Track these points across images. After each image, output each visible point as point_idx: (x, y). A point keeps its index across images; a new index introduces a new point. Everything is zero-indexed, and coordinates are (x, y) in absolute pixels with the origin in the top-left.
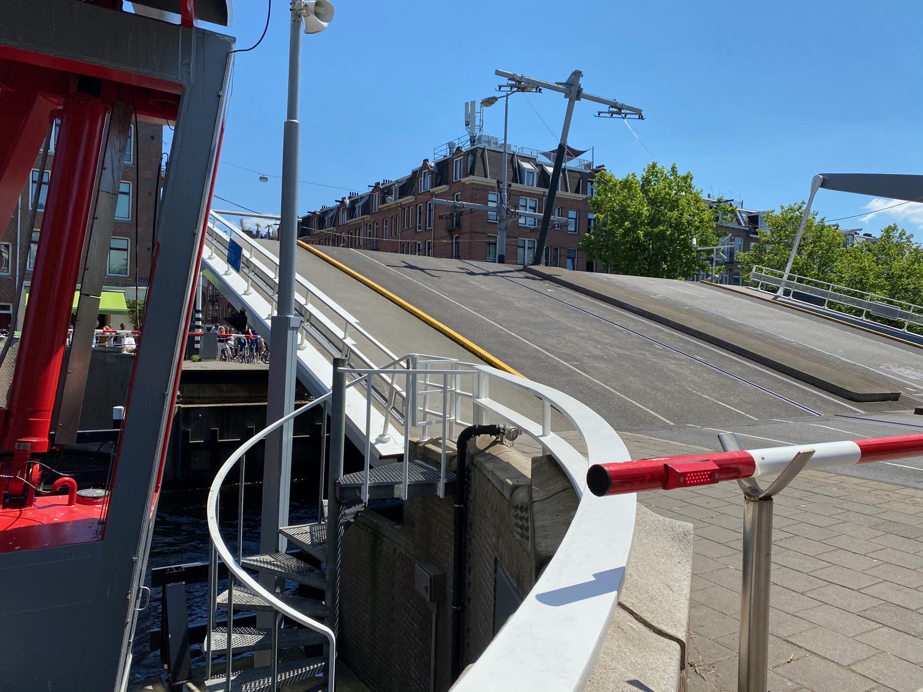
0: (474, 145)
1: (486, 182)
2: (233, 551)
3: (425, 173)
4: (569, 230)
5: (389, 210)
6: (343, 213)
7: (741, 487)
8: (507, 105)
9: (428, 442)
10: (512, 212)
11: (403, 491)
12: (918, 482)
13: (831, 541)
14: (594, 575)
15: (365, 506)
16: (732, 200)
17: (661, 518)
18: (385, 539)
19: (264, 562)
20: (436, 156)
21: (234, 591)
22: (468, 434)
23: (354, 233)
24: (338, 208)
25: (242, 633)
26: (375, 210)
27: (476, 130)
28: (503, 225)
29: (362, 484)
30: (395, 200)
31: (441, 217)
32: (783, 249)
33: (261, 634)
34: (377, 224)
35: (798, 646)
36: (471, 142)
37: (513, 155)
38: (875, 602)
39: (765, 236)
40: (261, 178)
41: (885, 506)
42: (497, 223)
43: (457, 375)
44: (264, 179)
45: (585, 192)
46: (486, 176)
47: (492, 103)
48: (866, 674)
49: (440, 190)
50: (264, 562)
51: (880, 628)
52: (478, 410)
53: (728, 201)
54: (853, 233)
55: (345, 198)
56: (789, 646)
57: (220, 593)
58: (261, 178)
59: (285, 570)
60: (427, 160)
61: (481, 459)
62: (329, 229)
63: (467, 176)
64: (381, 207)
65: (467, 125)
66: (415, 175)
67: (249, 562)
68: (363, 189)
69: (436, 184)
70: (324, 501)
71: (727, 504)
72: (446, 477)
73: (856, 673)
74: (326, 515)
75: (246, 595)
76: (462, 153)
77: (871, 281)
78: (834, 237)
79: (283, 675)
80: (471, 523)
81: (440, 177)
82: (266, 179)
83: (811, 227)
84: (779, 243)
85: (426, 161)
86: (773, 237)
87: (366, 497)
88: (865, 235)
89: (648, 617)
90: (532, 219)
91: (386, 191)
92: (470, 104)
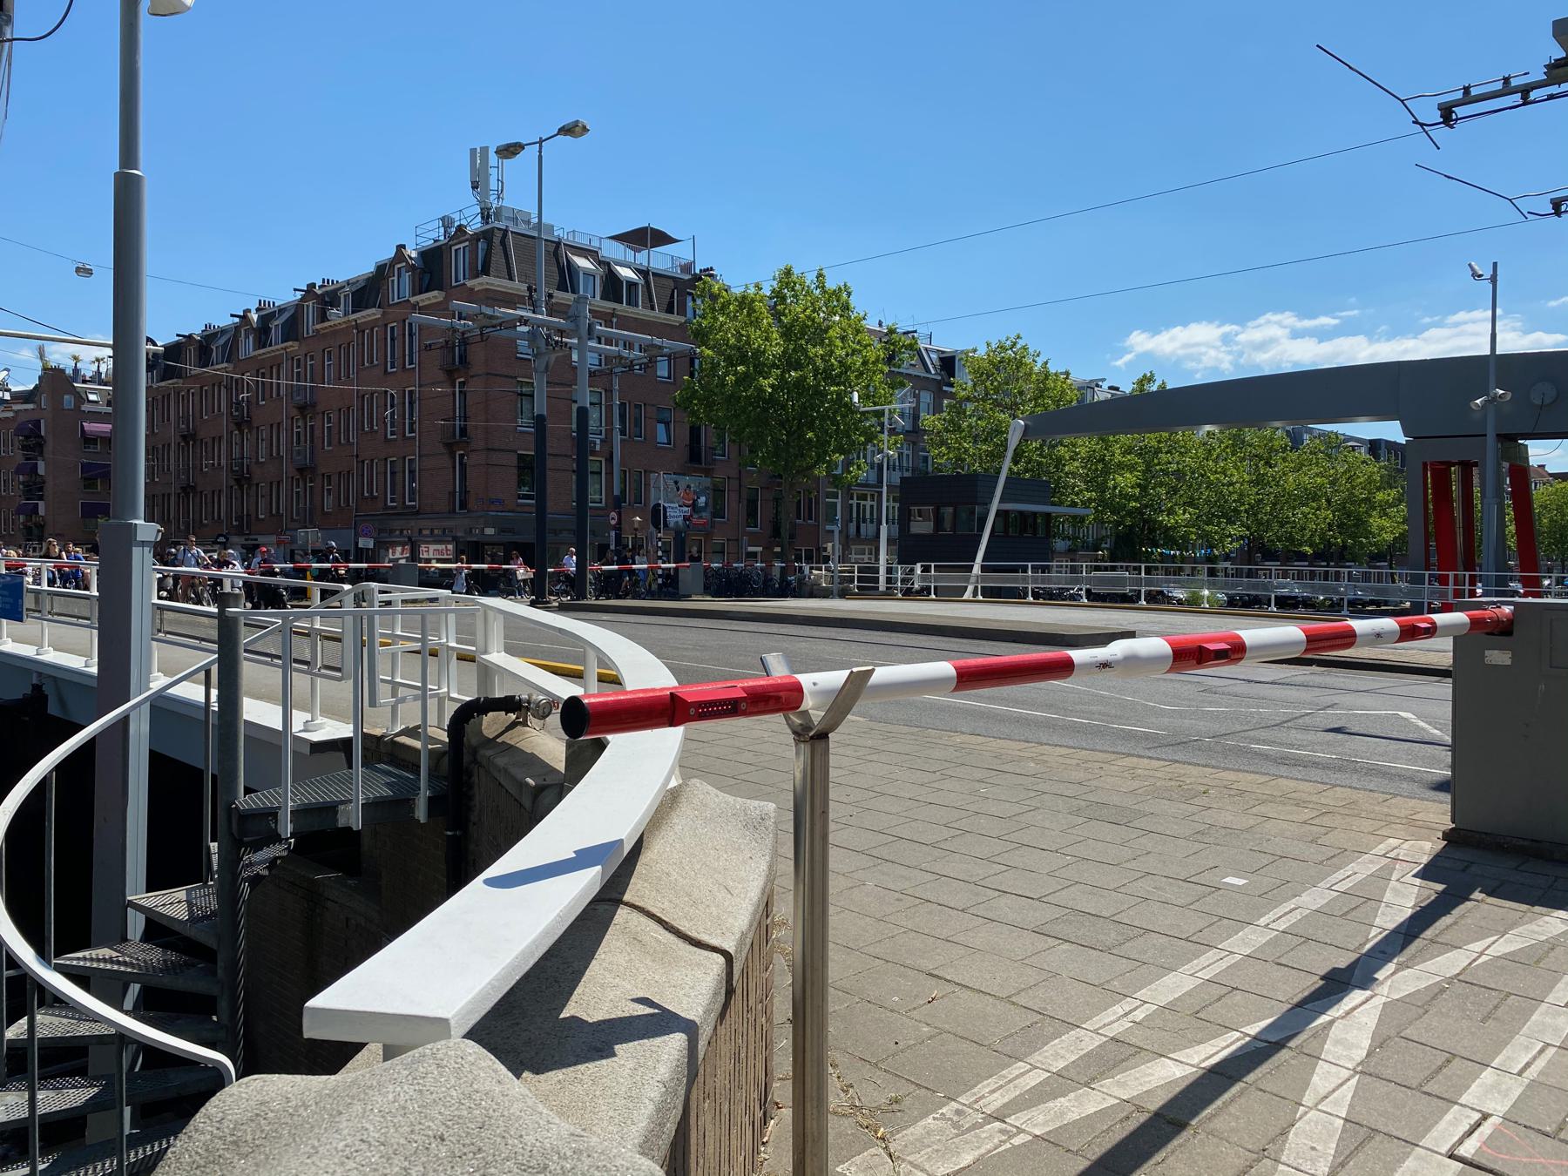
0: (487, 223)
1: (511, 288)
2: (41, 953)
3: (399, 269)
4: (659, 374)
5: (335, 332)
6: (247, 337)
7: (788, 724)
8: (540, 157)
9: (404, 732)
10: (557, 342)
11: (353, 815)
12: (1149, 749)
13: (1012, 837)
14: (575, 852)
15: (288, 848)
16: (915, 332)
17: (731, 799)
18: (329, 904)
19: (98, 960)
20: (419, 240)
21: (38, 1017)
22: (467, 714)
23: (268, 375)
24: (237, 328)
25: (58, 1088)
26: (308, 333)
27: (492, 198)
28: (541, 364)
29: (279, 808)
30: (345, 315)
31: (429, 347)
32: (991, 409)
33: (95, 1086)
34: (312, 359)
35: (946, 980)
36: (483, 218)
37: (558, 244)
38: (1058, 912)
39: (965, 389)
40: (78, 270)
41: (1094, 783)
42: (530, 360)
43: (449, 615)
44: (84, 271)
45: (682, 312)
46: (511, 278)
47: (515, 154)
48: (1030, 1005)
49: (429, 299)
50: (98, 960)
51: (1059, 945)
52: (487, 672)
53: (908, 332)
54: (1093, 385)
55: (249, 311)
56: (934, 981)
57: (11, 1022)
58: (78, 270)
59: (140, 969)
60: (403, 246)
61: (489, 753)
62: (218, 367)
63: (477, 277)
64: (318, 327)
65: (475, 186)
66: (382, 271)
67: (68, 962)
68: (285, 296)
69: (419, 289)
70: (212, 844)
71: (875, 794)
72: (430, 787)
73: (1018, 1005)
74: (215, 868)
75: (65, 1021)
76: (467, 236)
77: (1118, 458)
78: (1063, 391)
79: (141, 1151)
80: (474, 860)
81: (427, 277)
82: (89, 272)
83: (1030, 375)
84: (984, 400)
85: (401, 247)
86: (976, 391)
87: (287, 828)
88: (1110, 388)
89: (684, 926)
90: (596, 355)
91: (327, 299)
92: (478, 151)
